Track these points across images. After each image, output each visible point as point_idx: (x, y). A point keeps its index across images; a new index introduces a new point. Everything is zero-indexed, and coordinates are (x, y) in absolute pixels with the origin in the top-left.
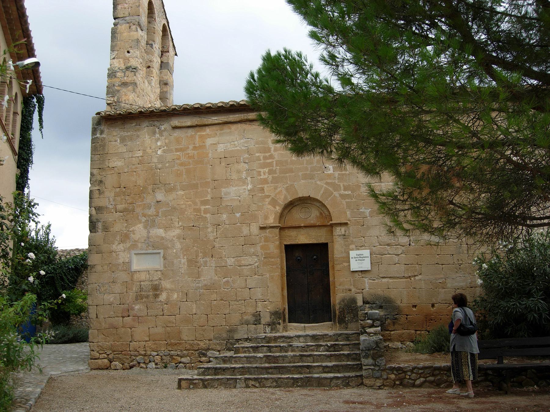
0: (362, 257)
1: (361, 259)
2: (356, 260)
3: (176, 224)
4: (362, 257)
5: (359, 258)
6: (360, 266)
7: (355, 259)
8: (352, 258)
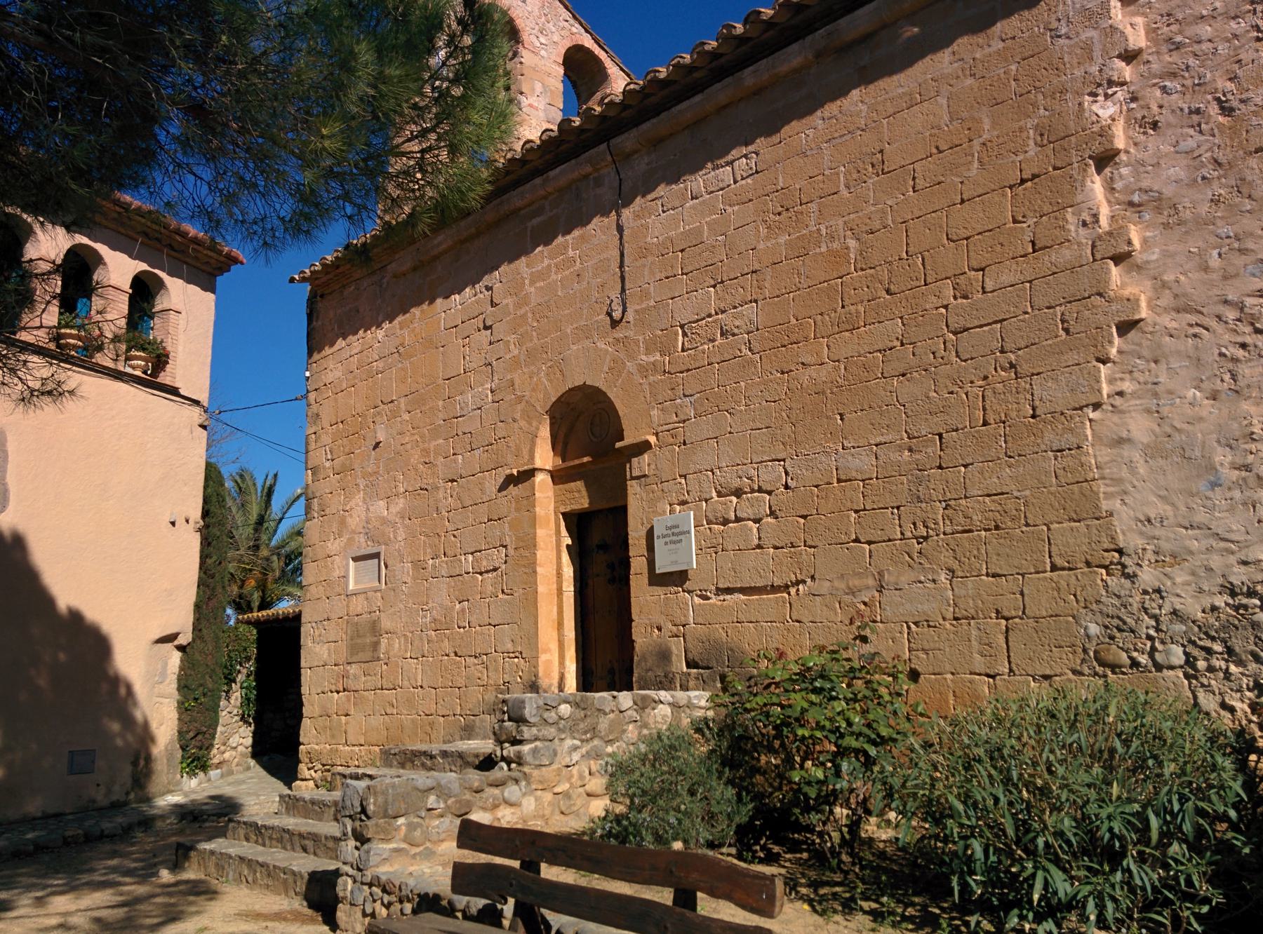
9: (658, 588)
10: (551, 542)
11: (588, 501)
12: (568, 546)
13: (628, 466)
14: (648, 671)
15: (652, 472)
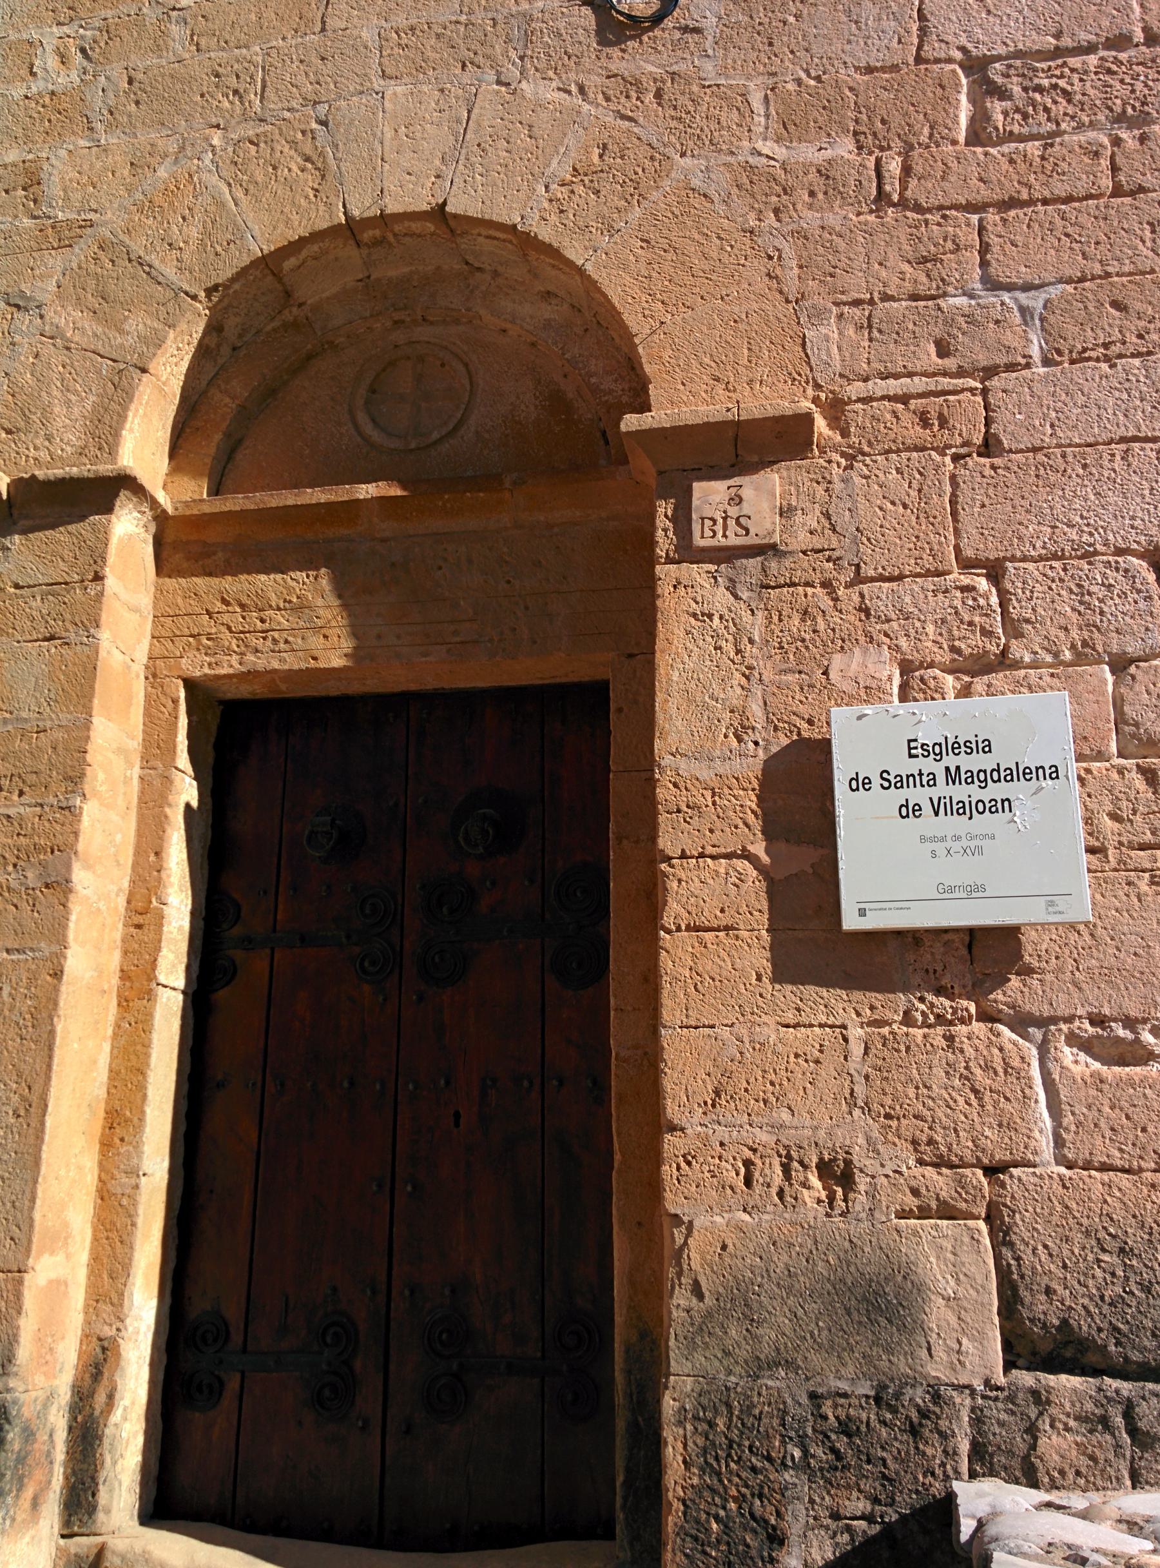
0: (982, 778)
1: (960, 792)
2: (909, 811)
3: (877, 1508)
4: (982, 778)
5: (942, 789)
6: (960, 871)
7: (898, 796)
8: (860, 783)
9: (835, 997)
10: (127, 781)
11: (347, 645)
12: (188, 806)
13: (664, 509)
14: (759, 1367)
15: (802, 539)
